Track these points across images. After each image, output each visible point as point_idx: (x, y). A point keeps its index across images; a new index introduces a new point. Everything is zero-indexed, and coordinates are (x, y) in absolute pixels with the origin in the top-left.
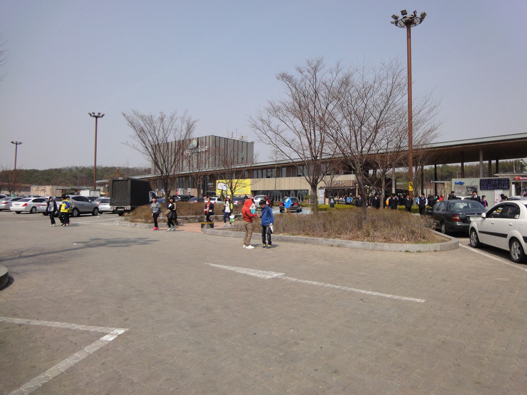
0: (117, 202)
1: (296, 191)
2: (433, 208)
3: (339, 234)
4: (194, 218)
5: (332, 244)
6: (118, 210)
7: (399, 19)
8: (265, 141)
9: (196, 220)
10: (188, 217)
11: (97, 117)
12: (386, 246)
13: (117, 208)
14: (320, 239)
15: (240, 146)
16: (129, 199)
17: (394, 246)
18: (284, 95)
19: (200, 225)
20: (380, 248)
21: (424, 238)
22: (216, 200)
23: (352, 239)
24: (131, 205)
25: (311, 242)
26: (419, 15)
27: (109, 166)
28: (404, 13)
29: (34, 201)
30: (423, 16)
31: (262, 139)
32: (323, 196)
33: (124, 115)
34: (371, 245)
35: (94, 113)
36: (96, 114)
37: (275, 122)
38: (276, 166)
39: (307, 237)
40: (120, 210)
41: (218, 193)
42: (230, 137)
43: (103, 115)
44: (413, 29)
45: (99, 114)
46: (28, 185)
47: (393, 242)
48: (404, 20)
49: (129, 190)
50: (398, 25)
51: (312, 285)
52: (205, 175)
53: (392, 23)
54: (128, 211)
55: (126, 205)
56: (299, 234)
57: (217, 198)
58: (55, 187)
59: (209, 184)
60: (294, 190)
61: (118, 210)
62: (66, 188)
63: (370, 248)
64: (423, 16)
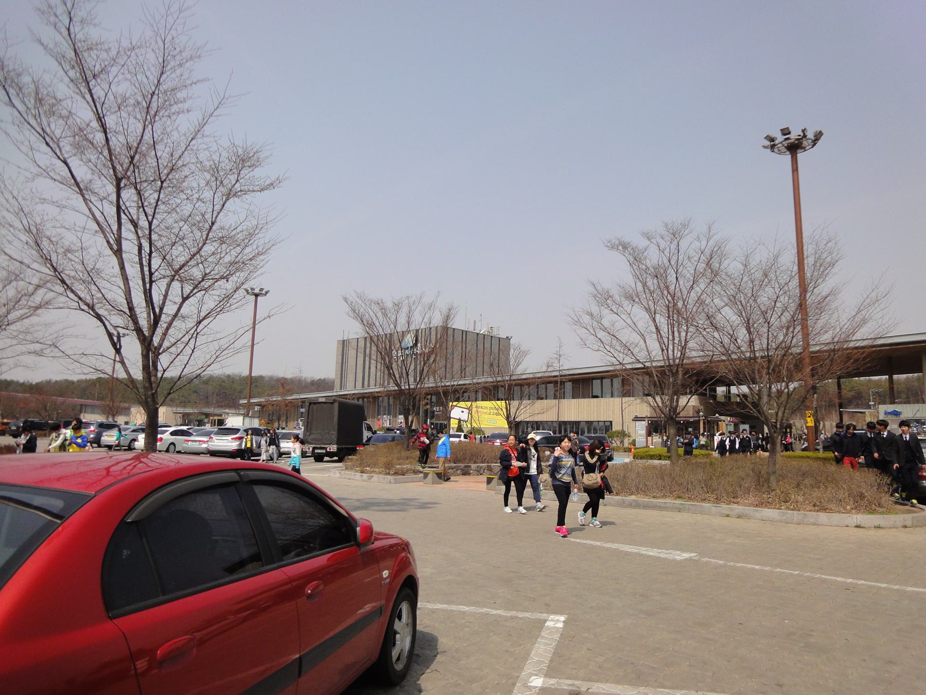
0: (314, 439)
1: (589, 423)
2: (737, 452)
3: (733, 497)
5: (728, 513)
7: (777, 142)
9: (459, 472)
11: (257, 295)
12: (823, 517)
14: (706, 505)
15: (487, 345)
17: (836, 518)
18: (618, 274)
19: (485, 480)
20: (812, 520)
21: (880, 505)
23: (761, 504)
25: (689, 510)
26: (810, 135)
27: (289, 375)
28: (786, 132)
29: (173, 434)
30: (818, 136)
31: (587, 342)
32: (644, 432)
33: (346, 300)
34: (796, 515)
35: (252, 289)
36: (257, 291)
37: (608, 318)
38: (559, 379)
39: (678, 502)
40: (320, 451)
41: (454, 424)
42: (471, 329)
43: (267, 293)
44: (801, 156)
45: (262, 290)
46: (127, 405)
47: (831, 511)
48: (786, 143)
50: (776, 150)
51: (753, 569)
52: (434, 392)
53: (765, 147)
56: (664, 496)
57: (463, 434)
58: (170, 409)
62: (188, 410)
63: (795, 520)
64: (818, 136)
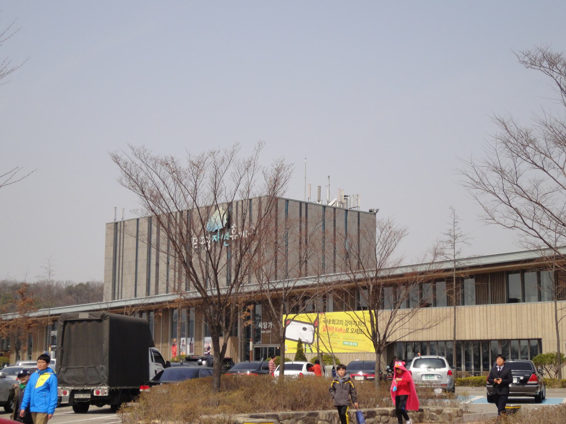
0: (73, 378)
4: (293, 416)
6: (77, 396)
8: (502, 221)
10: (279, 413)
13: (73, 392)
15: (340, 224)
16: (104, 369)
22: (304, 368)
24: (110, 384)
33: (116, 159)
40: (81, 396)
41: (290, 348)
42: (314, 200)
49: (106, 346)
54: (99, 401)
55: (97, 384)
57: (305, 364)
59: (260, 325)
60: (501, 341)
61: (77, 396)
